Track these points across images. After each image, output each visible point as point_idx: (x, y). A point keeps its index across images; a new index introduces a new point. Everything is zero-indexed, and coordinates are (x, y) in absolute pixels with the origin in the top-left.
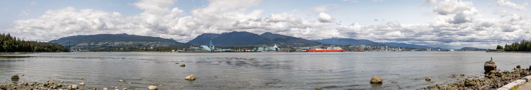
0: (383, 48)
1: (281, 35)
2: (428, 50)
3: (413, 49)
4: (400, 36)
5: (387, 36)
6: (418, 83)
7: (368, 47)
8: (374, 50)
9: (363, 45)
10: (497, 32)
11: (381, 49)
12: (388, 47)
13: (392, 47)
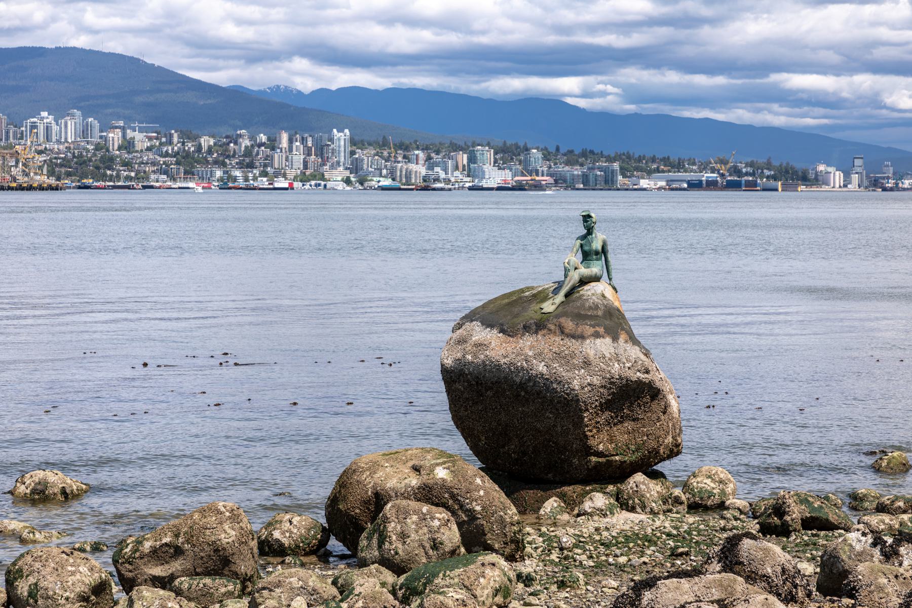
0: (298, 158)
1: (699, 119)
2: (837, 177)
3: (649, 173)
4: (477, 26)
5: (341, 20)
6: (846, 459)
7: (115, 137)
8: (189, 174)
9: (60, 113)
10: (884, 517)
11: (269, 159)
12: (353, 142)
13: (405, 147)
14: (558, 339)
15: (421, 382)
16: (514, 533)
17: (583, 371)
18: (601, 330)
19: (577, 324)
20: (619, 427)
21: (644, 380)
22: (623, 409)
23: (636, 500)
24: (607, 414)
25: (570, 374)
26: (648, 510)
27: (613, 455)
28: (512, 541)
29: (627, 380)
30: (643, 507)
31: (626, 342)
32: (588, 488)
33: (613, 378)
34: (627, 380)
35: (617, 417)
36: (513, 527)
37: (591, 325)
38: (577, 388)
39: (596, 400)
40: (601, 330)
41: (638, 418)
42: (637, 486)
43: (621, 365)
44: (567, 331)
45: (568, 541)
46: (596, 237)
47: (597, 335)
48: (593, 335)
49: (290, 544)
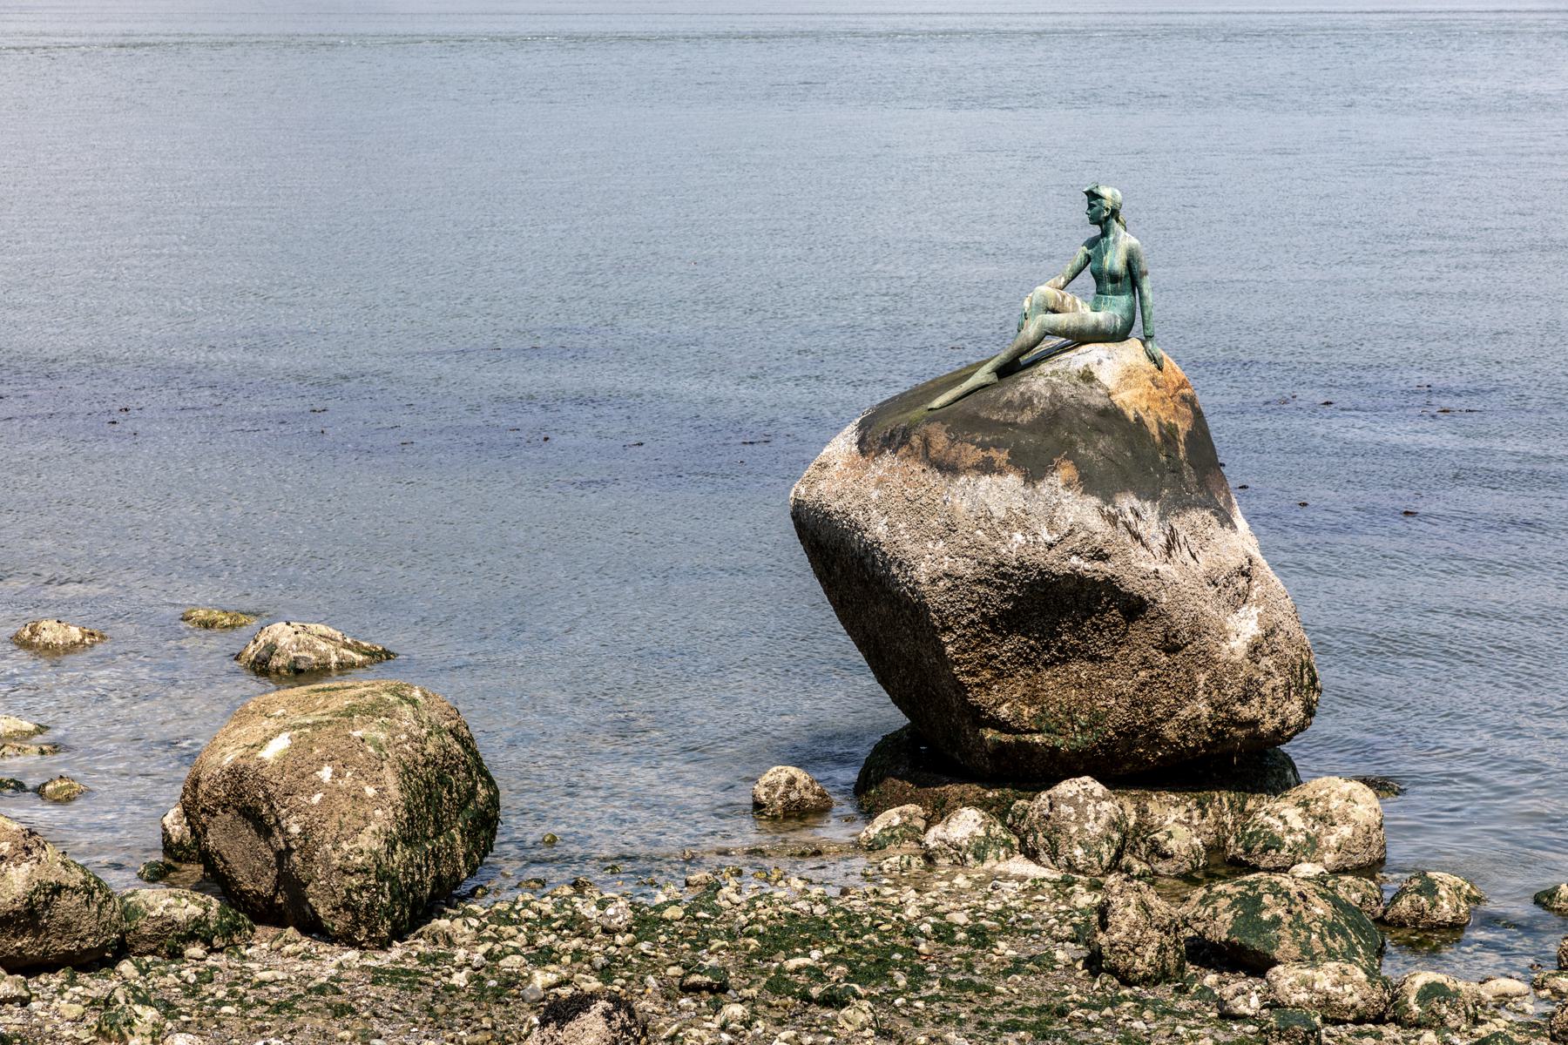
14: (917, 468)
16: (348, 891)
17: (941, 543)
18: (1001, 457)
19: (953, 441)
22: (1060, 634)
23: (1041, 840)
26: (1062, 861)
27: (1030, 732)
28: (346, 906)
29: (1040, 573)
30: (1054, 854)
32: (990, 795)
34: (1040, 573)
36: (347, 878)
37: (979, 445)
38: (923, 579)
39: (970, 610)
42: (1051, 805)
43: (1030, 538)
44: (932, 453)
45: (617, 916)
46: (1115, 241)
47: (987, 467)
48: (976, 467)
49: (183, 837)
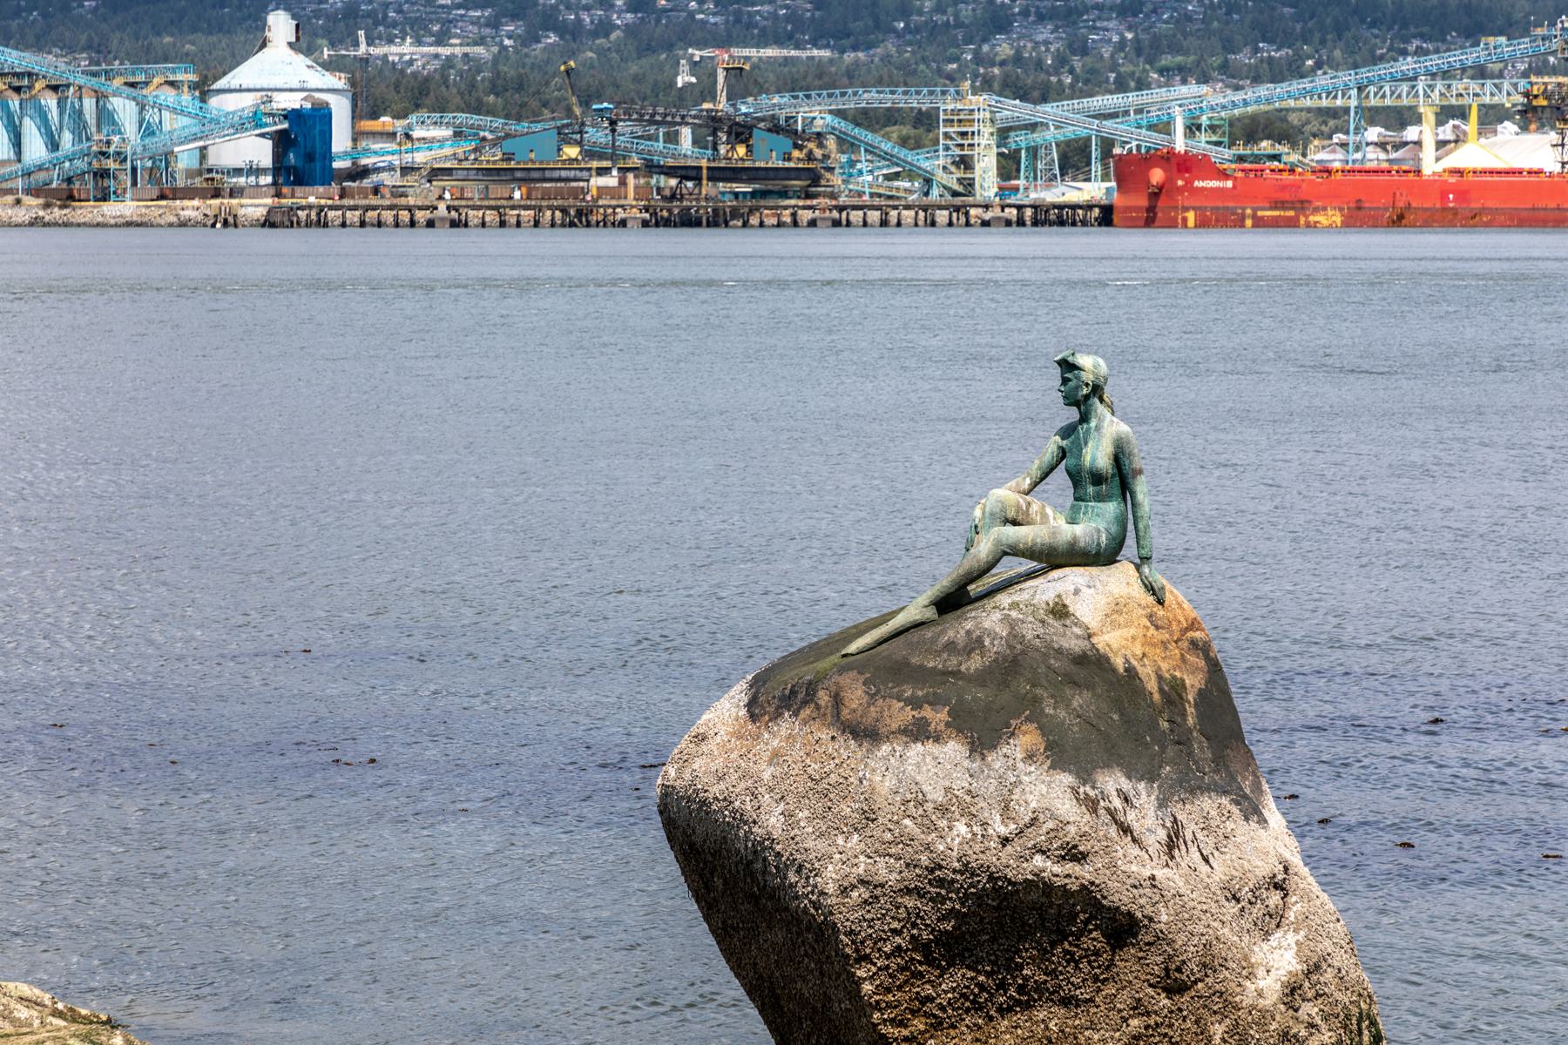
15: (1415, 978)
18: (938, 717)
20: (1019, 1018)
21: (1058, 882)
24: (958, 977)
25: (821, 846)
29: (991, 878)
31: (1030, 757)
33: (940, 867)
34: (991, 878)
35: (1002, 986)
38: (831, 888)
39: (895, 932)
40: (938, 717)
41: (1075, 998)
46: (1098, 428)
47: (919, 732)
48: (904, 731)
